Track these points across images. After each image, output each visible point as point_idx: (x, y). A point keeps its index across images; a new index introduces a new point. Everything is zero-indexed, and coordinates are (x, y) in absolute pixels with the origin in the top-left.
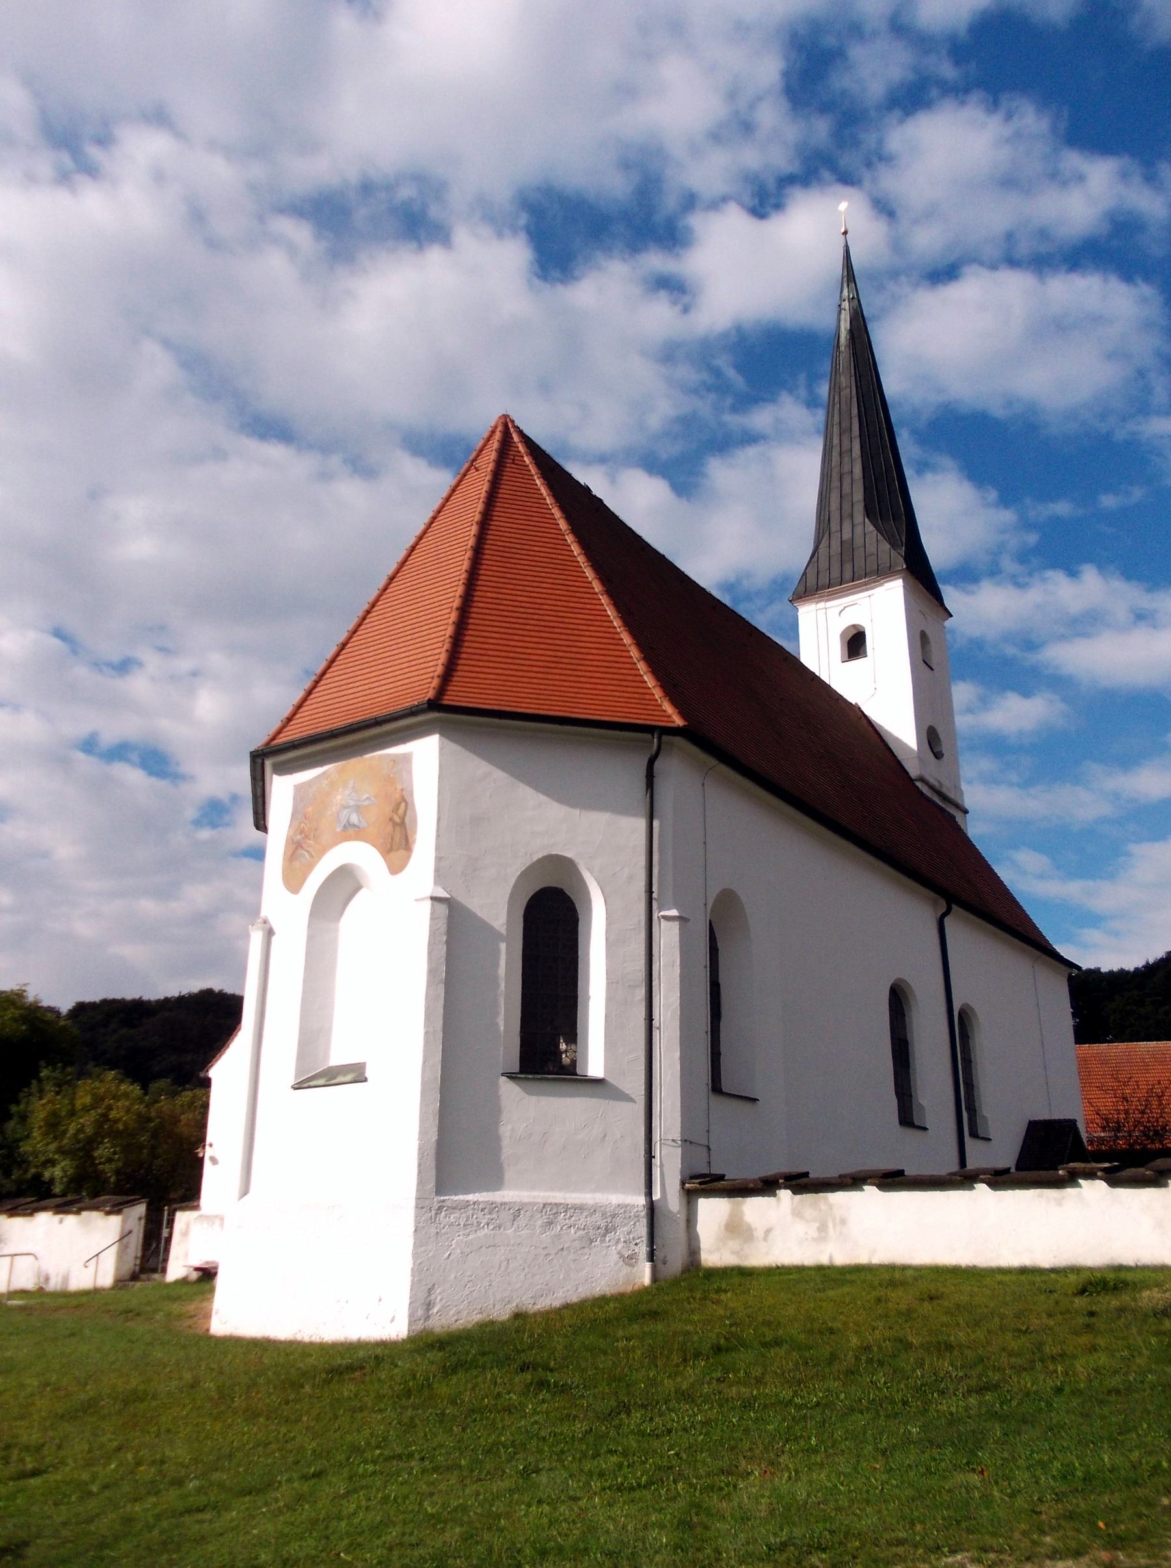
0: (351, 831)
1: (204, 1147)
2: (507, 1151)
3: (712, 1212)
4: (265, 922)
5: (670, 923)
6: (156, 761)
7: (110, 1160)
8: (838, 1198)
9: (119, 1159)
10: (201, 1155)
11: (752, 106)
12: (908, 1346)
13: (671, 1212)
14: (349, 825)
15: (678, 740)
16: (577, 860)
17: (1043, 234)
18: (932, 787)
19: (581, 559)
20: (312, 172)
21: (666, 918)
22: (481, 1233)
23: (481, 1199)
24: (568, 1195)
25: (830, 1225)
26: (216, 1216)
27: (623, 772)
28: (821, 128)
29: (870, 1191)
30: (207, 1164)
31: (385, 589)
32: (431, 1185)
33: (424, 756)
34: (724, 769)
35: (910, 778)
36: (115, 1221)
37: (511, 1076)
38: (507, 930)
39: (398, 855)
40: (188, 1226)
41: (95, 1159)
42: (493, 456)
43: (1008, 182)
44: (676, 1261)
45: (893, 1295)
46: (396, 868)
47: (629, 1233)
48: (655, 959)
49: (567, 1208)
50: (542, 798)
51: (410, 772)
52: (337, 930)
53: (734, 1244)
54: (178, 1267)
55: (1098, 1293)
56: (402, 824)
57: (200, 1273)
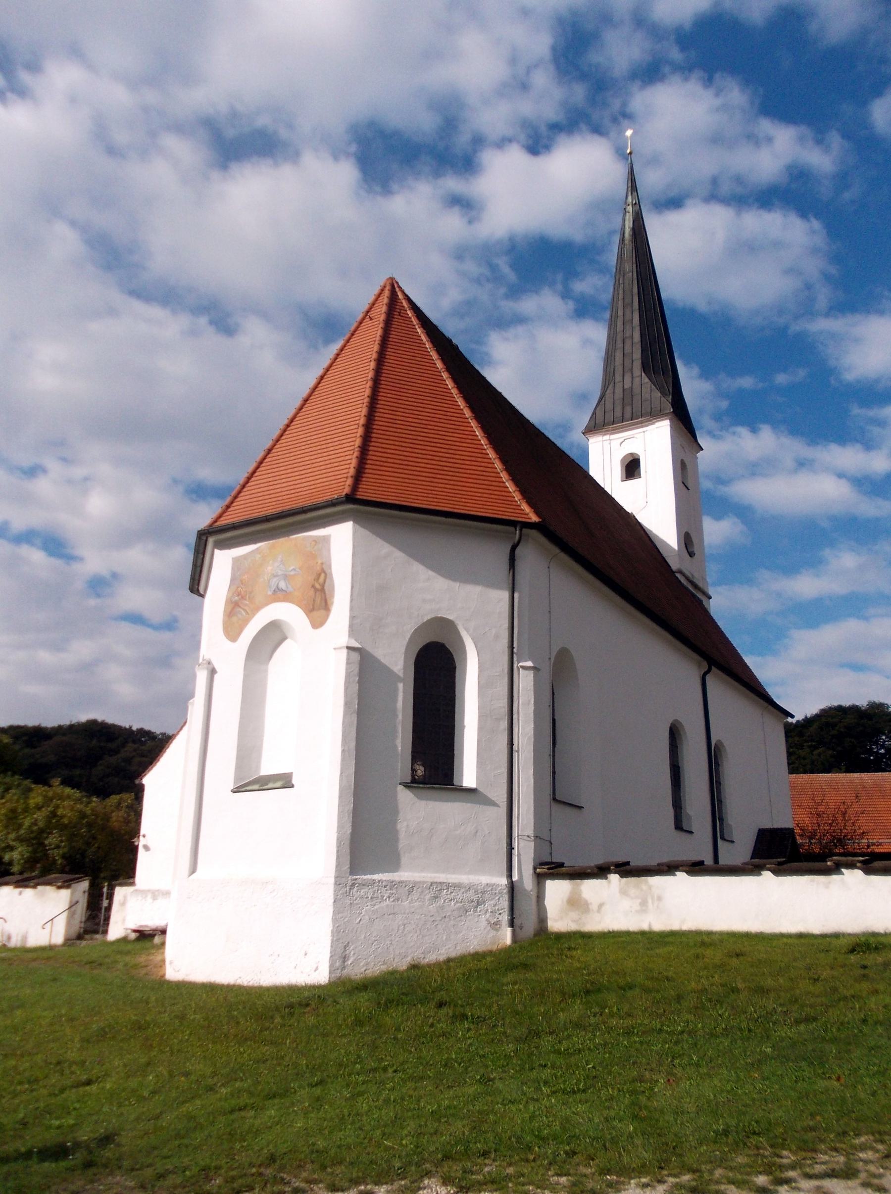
0: (280, 594)
2: (403, 843)
3: (557, 891)
4: (209, 663)
5: (527, 672)
6: (55, 545)
7: (58, 847)
8: (656, 881)
9: (65, 847)
11: (529, 70)
12: (735, 990)
13: (525, 890)
14: (278, 590)
15: (534, 533)
16: (457, 622)
17: (739, 180)
18: (687, 578)
19: (454, 391)
20: (199, 98)
21: (524, 668)
22: (384, 904)
23: (384, 879)
24: (449, 876)
25: (650, 901)
26: (149, 891)
27: (494, 554)
28: (579, 92)
29: (681, 876)
30: (141, 851)
31: (301, 409)
32: (346, 867)
33: (341, 539)
34: (563, 556)
36: (65, 894)
37: (407, 786)
38: (404, 673)
40: (125, 897)
41: (46, 846)
42: (384, 309)
43: (716, 139)
44: (529, 927)
45: (709, 952)
46: (317, 624)
47: (495, 906)
48: (515, 698)
49: (448, 886)
50: (431, 573)
51: (329, 550)
52: (266, 671)
53: (574, 915)
54: (116, 930)
55: (864, 952)
56: (323, 590)
57: (138, 934)
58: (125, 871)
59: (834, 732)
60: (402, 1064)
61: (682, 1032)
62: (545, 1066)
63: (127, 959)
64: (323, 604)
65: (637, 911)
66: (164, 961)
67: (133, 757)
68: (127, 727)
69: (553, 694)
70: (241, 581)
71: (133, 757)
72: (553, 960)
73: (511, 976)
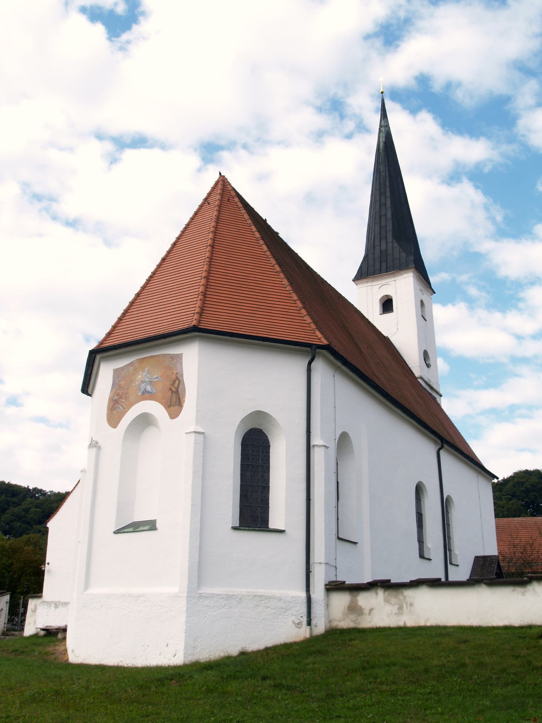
0: (147, 395)
1: (45, 564)
10: (43, 569)
12: (464, 665)
14: (145, 392)
15: (324, 351)
18: (426, 382)
25: (405, 606)
26: (52, 602)
35: (415, 377)
39: (174, 409)
40: (36, 606)
46: (173, 415)
53: (353, 617)
54: (29, 630)
56: (177, 392)
58: (36, 588)
59: (523, 489)
60: (242, 717)
61: (430, 693)
62: (340, 717)
63: (40, 648)
64: (178, 402)
65: (396, 614)
66: (66, 650)
67: (30, 508)
68: (26, 486)
69: (337, 464)
70: (120, 385)
71: (30, 508)
72: (339, 648)
73: (311, 659)
